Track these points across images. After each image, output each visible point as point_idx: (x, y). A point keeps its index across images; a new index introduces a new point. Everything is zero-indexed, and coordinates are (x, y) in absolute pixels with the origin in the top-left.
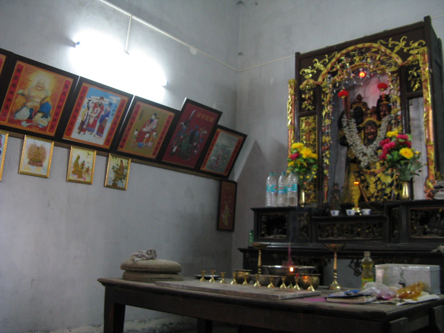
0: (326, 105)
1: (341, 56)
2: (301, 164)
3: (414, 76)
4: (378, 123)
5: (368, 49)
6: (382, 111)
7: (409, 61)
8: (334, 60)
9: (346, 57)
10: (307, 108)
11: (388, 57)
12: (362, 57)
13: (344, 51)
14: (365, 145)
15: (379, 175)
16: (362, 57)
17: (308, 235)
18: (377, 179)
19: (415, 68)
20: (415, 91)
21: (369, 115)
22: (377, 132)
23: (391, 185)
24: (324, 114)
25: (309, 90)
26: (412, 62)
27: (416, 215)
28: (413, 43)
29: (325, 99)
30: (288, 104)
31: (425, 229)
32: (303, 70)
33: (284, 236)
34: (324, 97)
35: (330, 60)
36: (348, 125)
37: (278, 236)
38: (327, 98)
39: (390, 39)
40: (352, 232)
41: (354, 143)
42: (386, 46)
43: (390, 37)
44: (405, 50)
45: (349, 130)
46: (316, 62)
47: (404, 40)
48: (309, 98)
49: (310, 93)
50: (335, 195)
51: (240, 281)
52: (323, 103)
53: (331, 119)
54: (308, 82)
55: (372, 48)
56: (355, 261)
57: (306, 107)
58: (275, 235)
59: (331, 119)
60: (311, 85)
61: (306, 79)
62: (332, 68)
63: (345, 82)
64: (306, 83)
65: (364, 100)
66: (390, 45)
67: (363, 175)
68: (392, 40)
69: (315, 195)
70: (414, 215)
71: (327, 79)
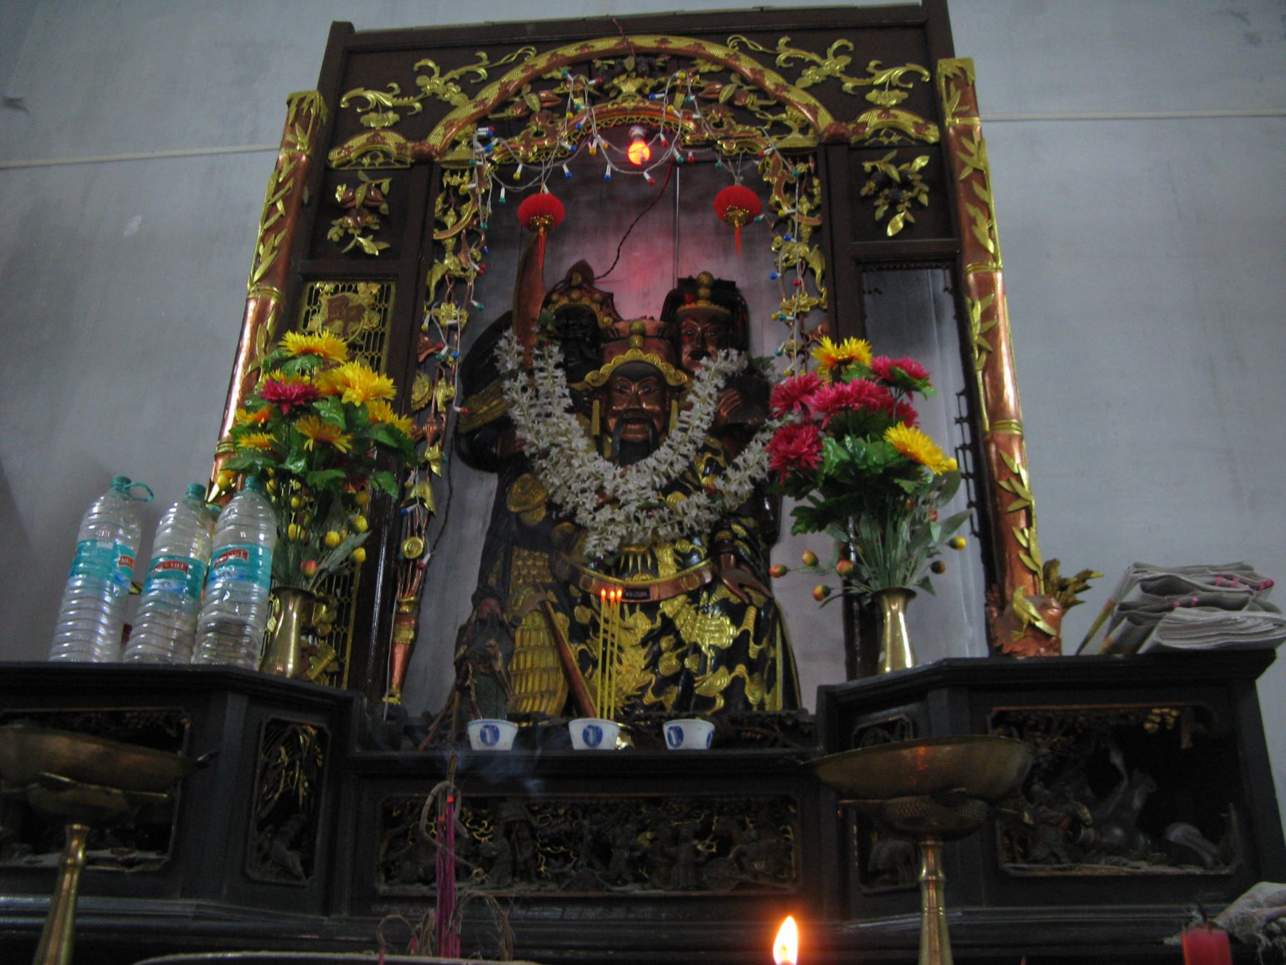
0: (450, 243)
2: (324, 445)
4: (673, 377)
5: (683, 60)
8: (516, 75)
12: (652, 82)
13: (571, 51)
16: (652, 82)
17: (307, 865)
20: (894, 237)
22: (666, 415)
23: (727, 657)
25: (374, 173)
26: (876, 133)
28: (878, 67)
29: (450, 219)
32: (358, 92)
35: (494, 74)
38: (459, 216)
39: (783, 41)
40: (602, 851)
42: (768, 60)
43: (784, 32)
46: (429, 72)
47: (841, 51)
49: (378, 186)
51: (780, 418)
52: (437, 235)
53: (470, 308)
54: (371, 141)
57: (347, 237)
59: (470, 308)
60: (387, 155)
61: (364, 129)
62: (503, 104)
63: (557, 164)
64: (363, 145)
68: (788, 45)
69: (338, 659)
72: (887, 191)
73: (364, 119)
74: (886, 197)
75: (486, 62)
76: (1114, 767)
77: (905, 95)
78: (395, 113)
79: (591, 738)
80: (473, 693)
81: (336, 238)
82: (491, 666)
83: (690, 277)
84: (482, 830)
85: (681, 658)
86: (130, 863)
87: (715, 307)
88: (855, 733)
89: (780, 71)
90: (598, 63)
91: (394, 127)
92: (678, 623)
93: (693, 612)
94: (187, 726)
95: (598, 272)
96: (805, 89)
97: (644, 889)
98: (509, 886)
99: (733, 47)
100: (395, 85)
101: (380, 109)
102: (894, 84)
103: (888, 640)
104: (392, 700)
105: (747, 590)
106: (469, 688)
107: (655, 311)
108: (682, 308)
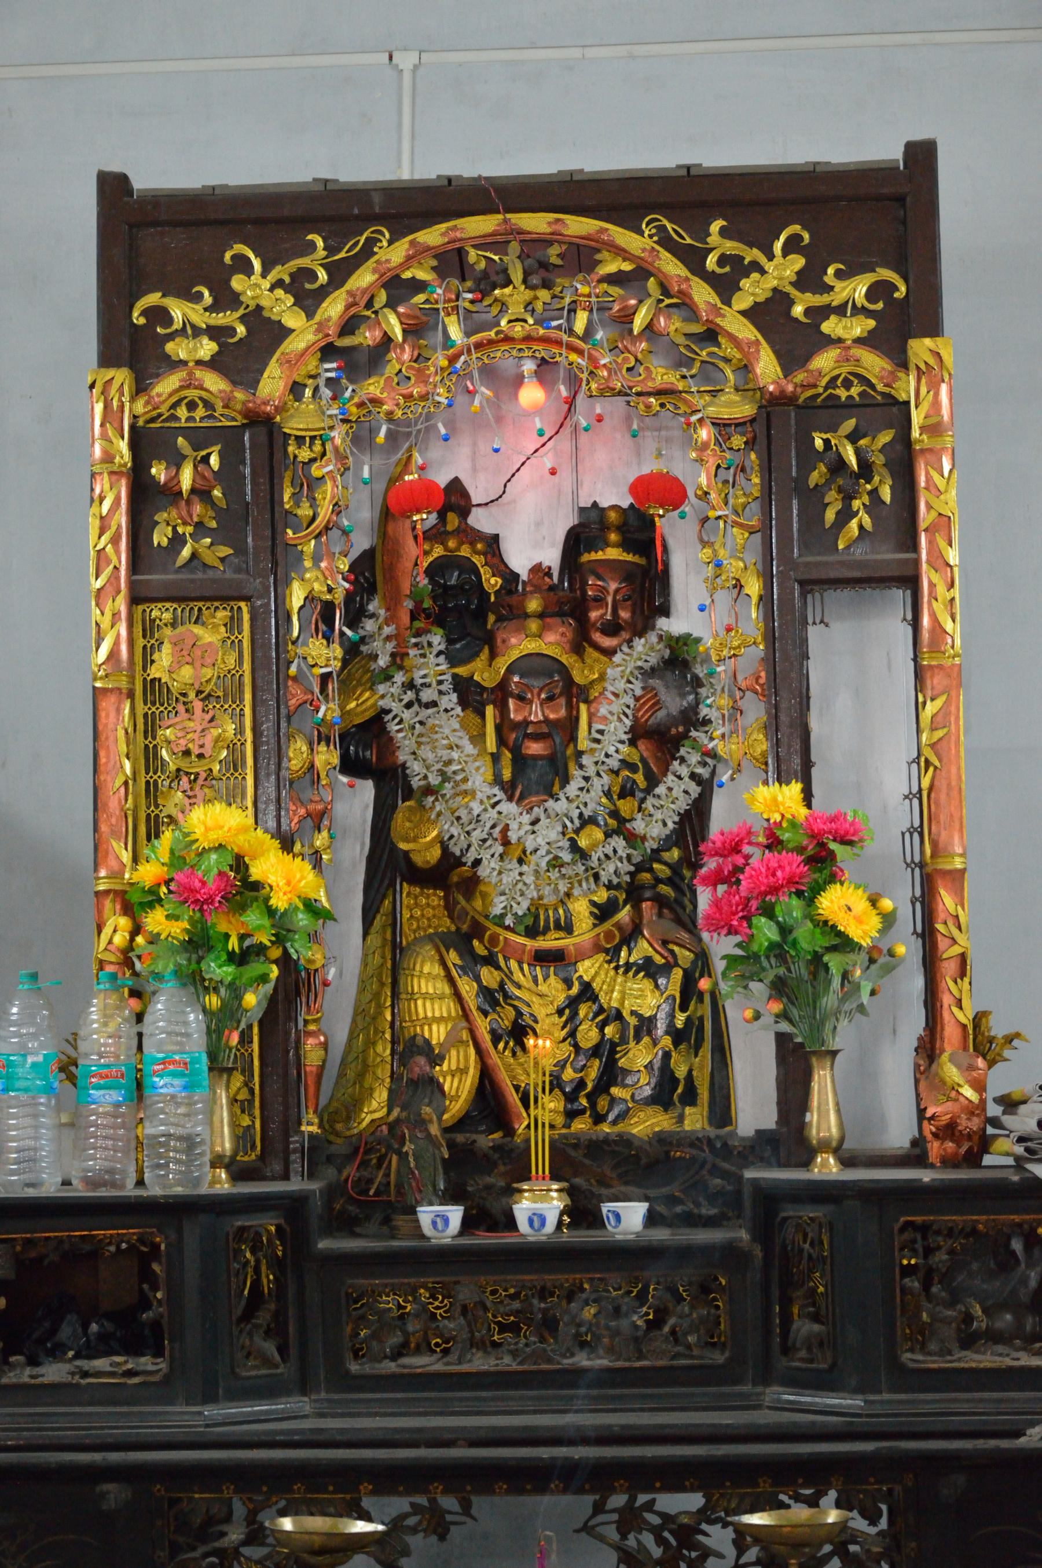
1: (409, 261)
3: (839, 465)
6: (599, 601)
7: (820, 373)
8: (364, 278)
9: (441, 272)
10: (186, 552)
11: (696, 328)
13: (432, 236)
14: (509, 789)
15: (586, 969)
17: (282, 1350)
18: (575, 990)
19: (850, 424)
21: (534, 625)
22: (572, 723)
24: (297, 597)
27: (928, 1252)
28: (839, 275)
29: (305, 511)
30: (94, 524)
31: (968, 1318)
32: (153, 299)
33: (146, 1362)
34: (296, 497)
35: (340, 273)
36: (398, 659)
37: (101, 1364)
39: (716, 226)
41: (445, 778)
44: (798, 310)
45: (410, 695)
46: (243, 266)
47: (792, 246)
48: (201, 492)
50: (427, 1110)
55: (605, 255)
56: (618, 1500)
57: (177, 541)
58: (77, 1356)
62: (350, 325)
65: (480, 520)
66: (711, 262)
67: (490, 960)
69: (247, 1084)
70: (919, 1246)
71: (316, 389)
72: (840, 481)
73: (170, 347)
74: (840, 490)
75: (321, 253)
76: (1013, 1253)
77: (871, 323)
78: (211, 339)
79: (536, 1224)
80: (411, 1159)
81: (165, 542)
82: (427, 1130)
83: (595, 504)
84: (437, 1303)
85: (601, 1027)
86: (130, 1373)
87: (629, 557)
88: (779, 1219)
89: (710, 279)
90: (473, 255)
91: (213, 364)
92: (594, 985)
93: (612, 973)
94: (163, 1247)
95: (477, 496)
96: (743, 313)
97: (589, 1359)
98: (470, 1361)
99: (651, 236)
100: (206, 293)
101: (189, 331)
102: (859, 305)
103: (815, 1104)
104: (310, 1128)
105: (671, 946)
106: (407, 1153)
107: (551, 557)
108: (586, 557)
